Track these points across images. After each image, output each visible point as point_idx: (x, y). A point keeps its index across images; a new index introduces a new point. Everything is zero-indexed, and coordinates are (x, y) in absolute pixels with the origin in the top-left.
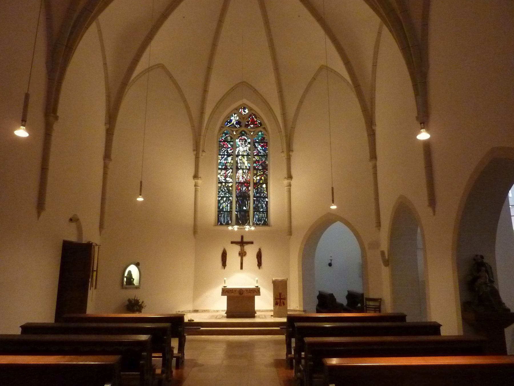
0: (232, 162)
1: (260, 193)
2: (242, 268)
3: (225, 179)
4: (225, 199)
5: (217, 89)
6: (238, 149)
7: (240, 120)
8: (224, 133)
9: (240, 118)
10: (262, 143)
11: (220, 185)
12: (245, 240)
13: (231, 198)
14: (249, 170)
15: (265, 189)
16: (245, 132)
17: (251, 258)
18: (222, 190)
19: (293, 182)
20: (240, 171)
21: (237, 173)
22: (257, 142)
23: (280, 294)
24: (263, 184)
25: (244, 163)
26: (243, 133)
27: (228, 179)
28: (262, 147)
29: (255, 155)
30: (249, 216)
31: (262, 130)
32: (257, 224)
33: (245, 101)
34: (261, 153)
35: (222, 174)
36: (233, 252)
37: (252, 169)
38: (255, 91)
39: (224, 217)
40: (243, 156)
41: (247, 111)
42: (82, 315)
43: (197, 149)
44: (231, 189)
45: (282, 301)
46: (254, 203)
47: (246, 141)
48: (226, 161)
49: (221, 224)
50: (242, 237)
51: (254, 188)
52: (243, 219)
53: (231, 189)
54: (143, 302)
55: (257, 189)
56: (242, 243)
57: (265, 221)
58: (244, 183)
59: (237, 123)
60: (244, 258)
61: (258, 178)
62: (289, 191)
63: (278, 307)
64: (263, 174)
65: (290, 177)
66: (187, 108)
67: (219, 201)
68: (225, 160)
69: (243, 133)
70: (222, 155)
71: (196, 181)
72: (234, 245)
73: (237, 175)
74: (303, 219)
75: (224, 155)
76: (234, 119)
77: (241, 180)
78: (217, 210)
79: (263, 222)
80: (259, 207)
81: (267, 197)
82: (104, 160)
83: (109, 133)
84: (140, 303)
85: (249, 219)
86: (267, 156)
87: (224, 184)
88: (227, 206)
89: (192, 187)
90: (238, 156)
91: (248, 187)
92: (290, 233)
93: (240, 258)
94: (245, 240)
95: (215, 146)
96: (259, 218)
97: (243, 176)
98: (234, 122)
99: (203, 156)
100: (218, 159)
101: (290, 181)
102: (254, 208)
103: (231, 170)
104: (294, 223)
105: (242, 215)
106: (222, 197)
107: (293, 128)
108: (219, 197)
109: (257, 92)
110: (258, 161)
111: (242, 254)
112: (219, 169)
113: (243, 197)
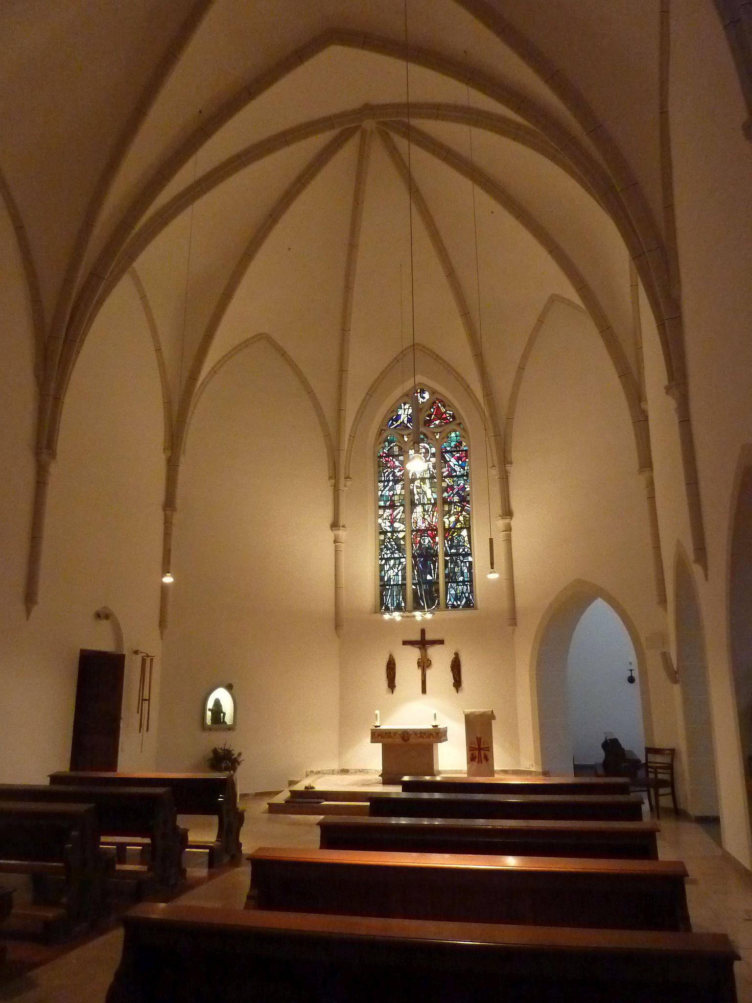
0: (403, 492)
1: (457, 547)
2: (424, 691)
3: (392, 526)
4: (392, 562)
5: (363, 367)
8: (386, 440)
10: (458, 452)
11: (382, 537)
12: (429, 637)
13: (403, 560)
14: (434, 505)
15: (466, 539)
16: (425, 435)
17: (440, 673)
18: (386, 547)
19: (515, 522)
20: (419, 509)
21: (412, 512)
22: (447, 452)
23: (479, 740)
24: (461, 529)
25: (425, 493)
26: (422, 436)
27: (396, 525)
29: (445, 477)
30: (437, 591)
31: (455, 428)
33: (420, 379)
34: (456, 471)
35: (385, 516)
36: (407, 662)
37: (439, 503)
38: (438, 358)
39: (392, 595)
40: (423, 480)
41: (427, 395)
42: (110, 775)
43: (336, 475)
44: (402, 542)
45: (482, 753)
46: (446, 566)
47: (427, 451)
48: (391, 493)
49: (387, 609)
50: (423, 632)
51: (445, 538)
52: (427, 596)
53: (402, 542)
55: (452, 540)
56: (423, 643)
57: (468, 599)
58: (427, 530)
60: (428, 672)
61: (453, 519)
63: (475, 763)
64: (461, 512)
65: (508, 513)
67: (382, 568)
70: (384, 481)
71: (337, 532)
72: (409, 647)
73: (414, 515)
75: (389, 481)
76: (405, 413)
77: (422, 525)
78: (378, 583)
79: (464, 600)
80: (455, 573)
81: (470, 555)
82: (164, 510)
83: (172, 465)
84: (236, 756)
85: (438, 597)
86: (467, 476)
87: (389, 535)
88: (397, 574)
89: (330, 547)
90: (413, 481)
91: (433, 538)
92: (513, 621)
93: (420, 672)
94: (429, 637)
95: (370, 468)
96: (456, 594)
97: (423, 518)
98: (404, 418)
99: (345, 487)
100: (377, 489)
101: (507, 521)
102: (447, 576)
103: (401, 508)
104: (520, 601)
106: (388, 560)
107: (510, 418)
108: (381, 559)
109: (441, 358)
111: (424, 664)
112: (380, 507)
113: (425, 557)
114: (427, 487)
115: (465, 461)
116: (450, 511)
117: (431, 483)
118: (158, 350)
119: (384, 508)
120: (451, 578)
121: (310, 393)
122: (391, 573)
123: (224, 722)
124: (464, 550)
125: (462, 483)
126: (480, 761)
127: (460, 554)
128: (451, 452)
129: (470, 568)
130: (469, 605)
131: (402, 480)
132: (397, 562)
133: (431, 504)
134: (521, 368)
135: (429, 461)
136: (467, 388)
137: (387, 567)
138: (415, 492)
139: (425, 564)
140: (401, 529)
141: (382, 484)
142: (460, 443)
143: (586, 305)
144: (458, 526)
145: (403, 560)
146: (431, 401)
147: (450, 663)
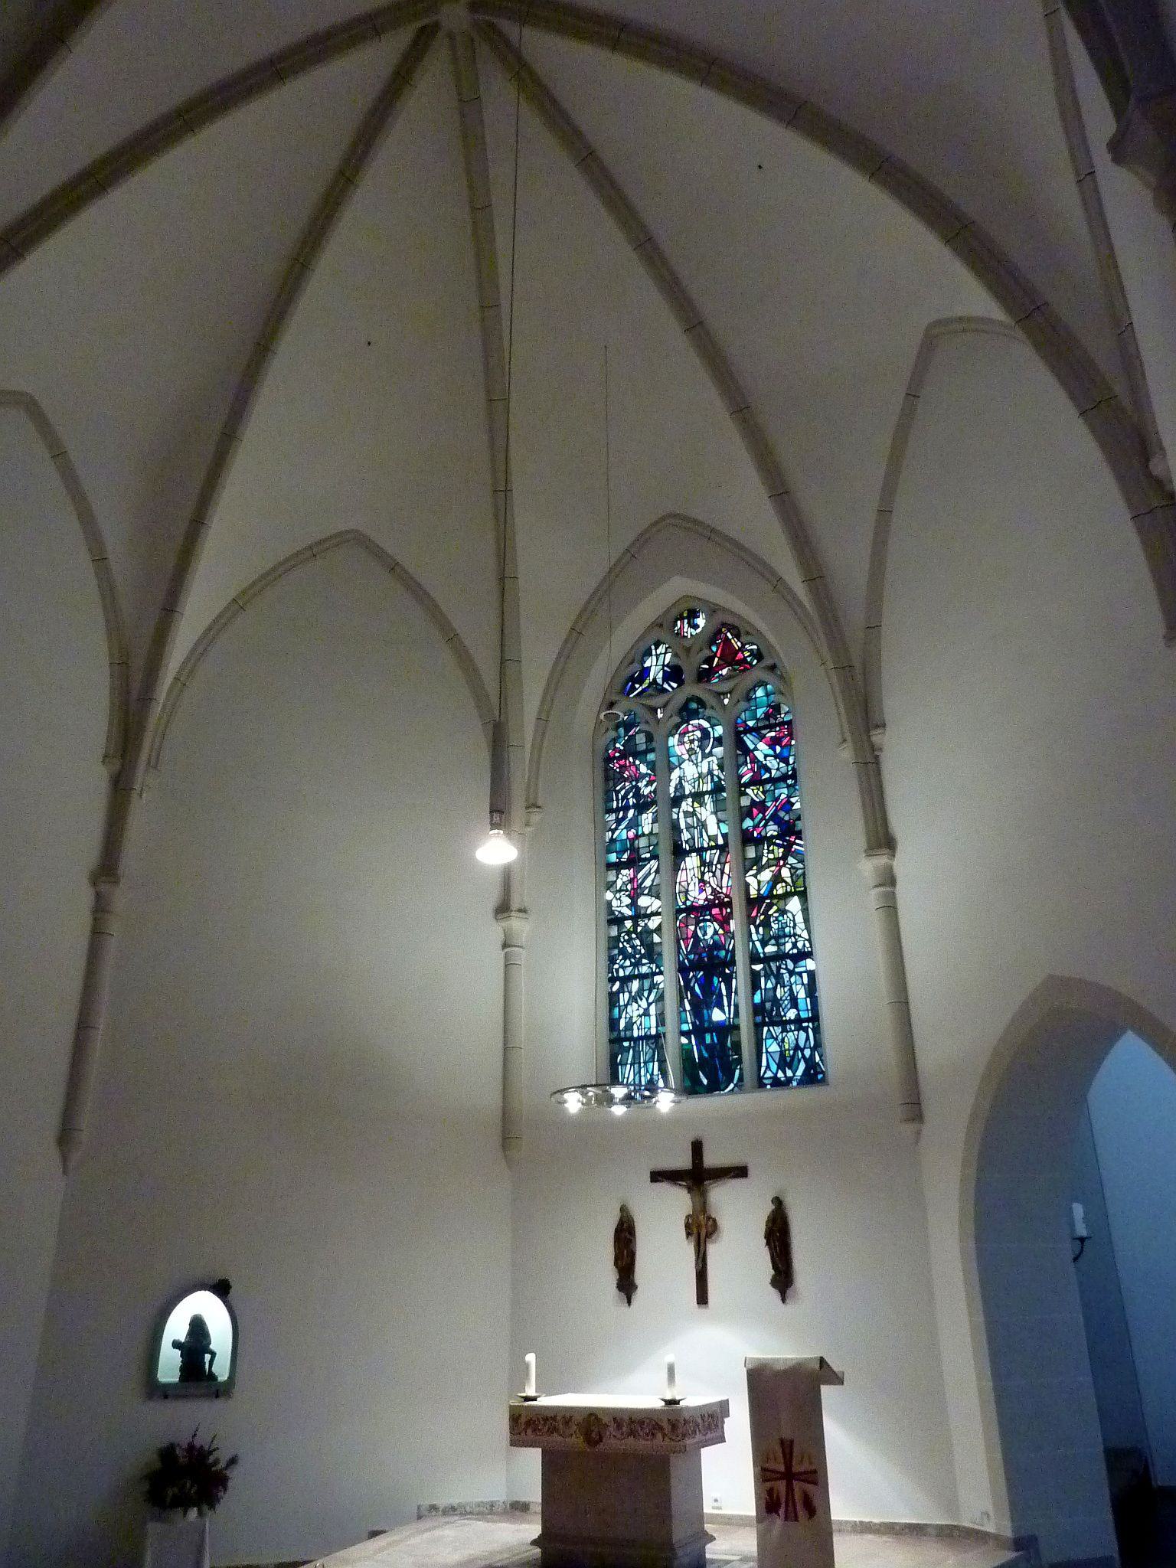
1: (778, 938)
2: (702, 1298)
3: (634, 905)
4: (635, 985)
5: (556, 566)
6: (675, 775)
7: (676, 661)
9: (675, 655)
10: (771, 727)
12: (710, 1160)
14: (723, 849)
15: (799, 918)
17: (739, 1251)
18: (622, 952)
19: (904, 864)
20: (692, 861)
21: (676, 868)
22: (749, 730)
23: (787, 1447)
24: (787, 896)
25: (703, 825)
26: (694, 706)
27: (643, 901)
28: (772, 746)
29: (747, 785)
30: (737, 1047)
32: (776, 1083)
34: (768, 770)
35: (619, 883)
36: (663, 1216)
38: (711, 534)
39: (636, 1061)
40: (698, 796)
41: (701, 621)
45: (797, 1485)
46: (755, 986)
48: (631, 834)
50: (697, 1148)
51: (751, 920)
53: (656, 939)
54: (233, 1461)
55: (766, 924)
56: (697, 1176)
57: (810, 1064)
59: (667, 678)
60: (713, 1250)
61: (766, 875)
62: (890, 908)
63: (779, 1522)
64: (784, 858)
65: (882, 841)
66: (464, 657)
67: (613, 998)
68: (628, 828)
69: (694, 706)
70: (617, 810)
71: (504, 924)
72: (665, 1187)
73: (681, 876)
74: (958, 1041)
75: (626, 808)
77: (698, 897)
79: (802, 1066)
80: (776, 1002)
81: (808, 955)
85: (739, 1061)
86: (794, 776)
87: (628, 924)
88: (646, 1013)
90: (676, 802)
91: (724, 922)
92: (914, 1109)
93: (689, 1250)
94: (710, 1160)
96: (782, 1054)
97: (702, 880)
98: (656, 673)
101: (882, 860)
102: (757, 1009)
104: (929, 1058)
105: (708, 1048)
107: (873, 628)
108: (612, 980)
110: (761, 806)
111: (701, 1230)
112: (610, 866)
113: (707, 968)
114: (706, 813)
115: (788, 745)
116: (757, 860)
117: (715, 802)
118: (100, 560)
119: (618, 866)
120: (766, 1014)
121: (452, 639)
122: (634, 1011)
123: (212, 1377)
124: (795, 945)
125: (783, 793)
126: (791, 1516)
127: (787, 956)
128: (756, 731)
129: (811, 989)
130: (813, 1076)
131: (653, 803)
132: (647, 983)
133: (717, 847)
134: (885, 513)
135: (711, 754)
136: (778, 584)
137: (624, 998)
138: (683, 825)
139: (707, 985)
140: (654, 908)
141: (613, 817)
142: (777, 708)
143: (1009, 311)
144: (780, 890)
145: (658, 979)
146: (712, 629)
147: (763, 1227)
